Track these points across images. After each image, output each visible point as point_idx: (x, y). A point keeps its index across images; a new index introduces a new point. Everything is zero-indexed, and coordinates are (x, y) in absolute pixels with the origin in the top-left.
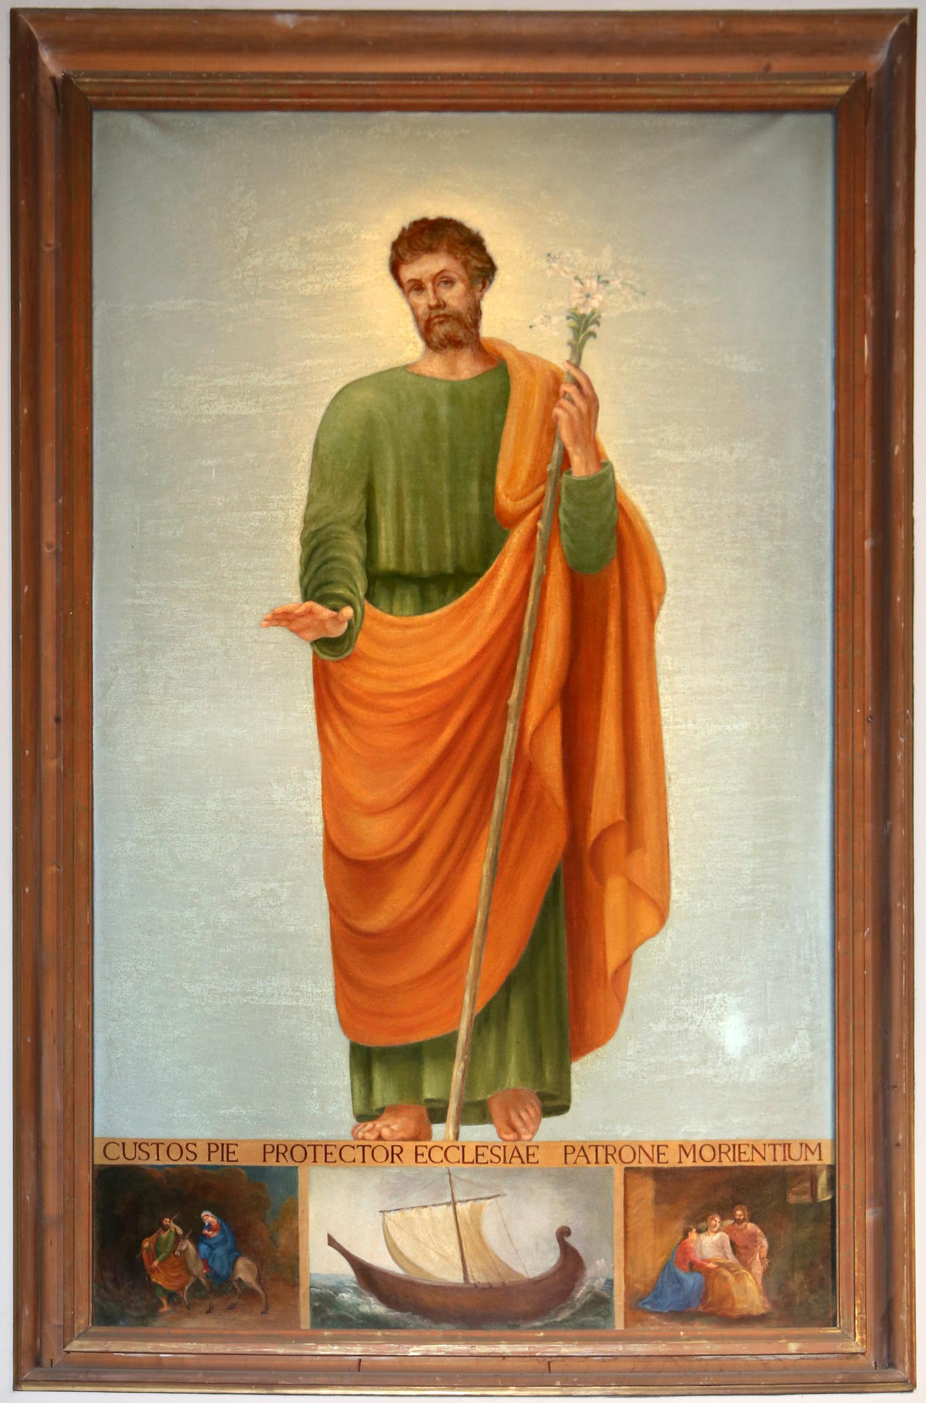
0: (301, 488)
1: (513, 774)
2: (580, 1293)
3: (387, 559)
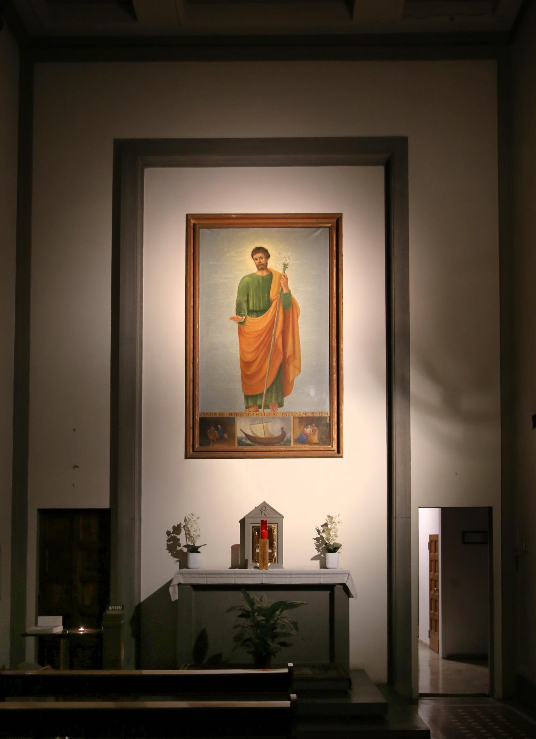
0: (236, 295)
1: (273, 346)
2: (285, 439)
3: (251, 307)
